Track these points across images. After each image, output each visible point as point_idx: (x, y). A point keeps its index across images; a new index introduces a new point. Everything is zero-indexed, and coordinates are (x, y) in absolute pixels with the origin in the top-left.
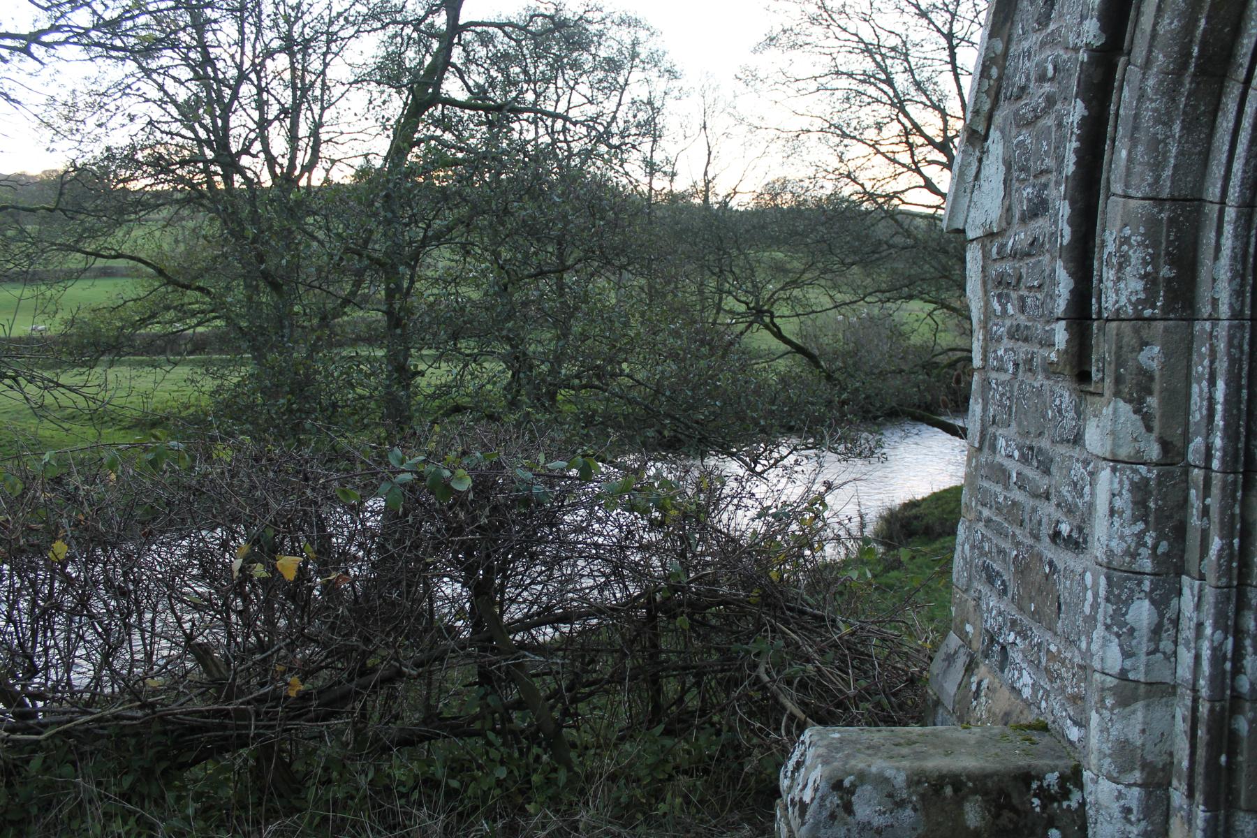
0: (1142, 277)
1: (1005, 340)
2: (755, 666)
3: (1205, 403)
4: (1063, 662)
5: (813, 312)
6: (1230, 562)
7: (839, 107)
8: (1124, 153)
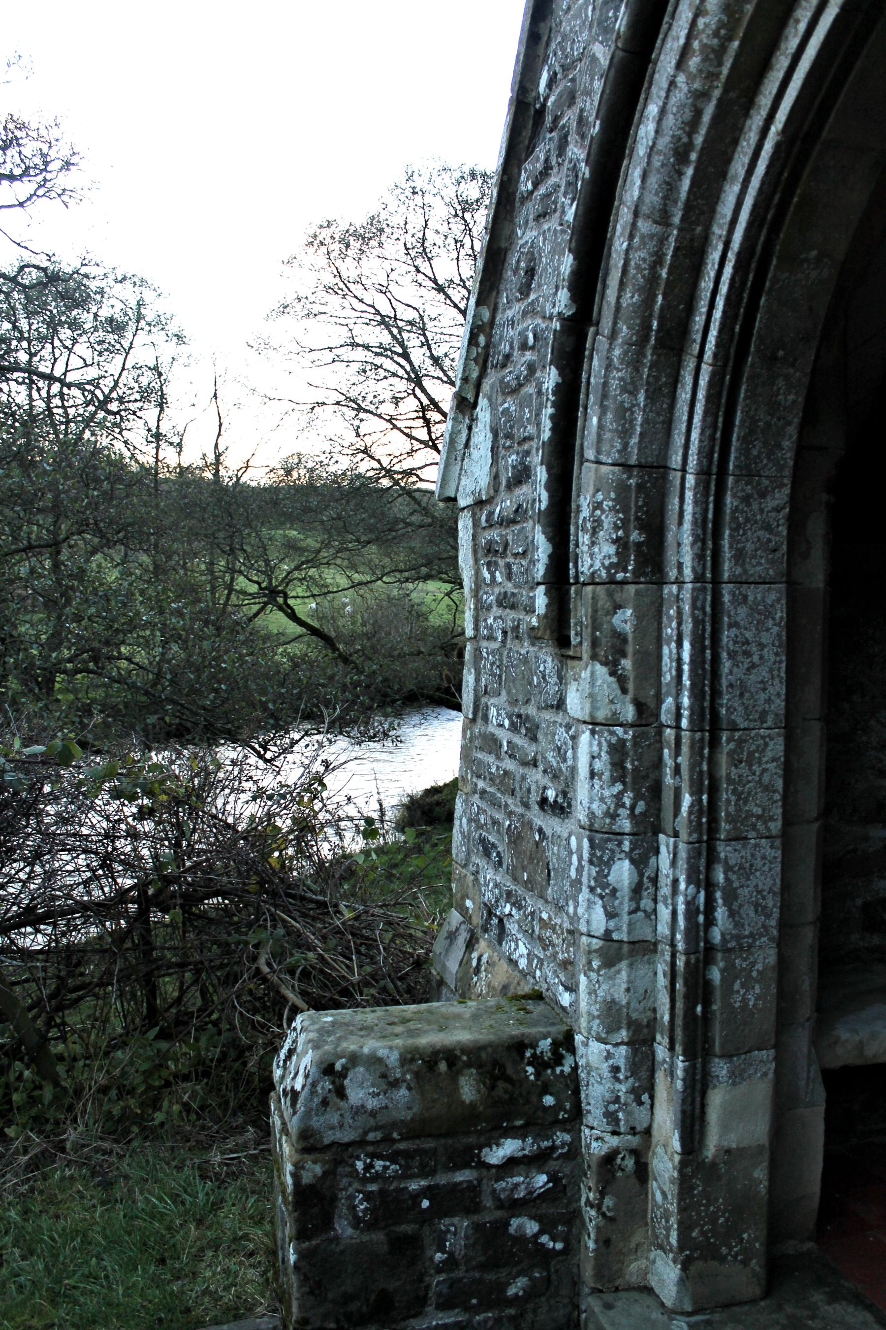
0: (614, 542)
1: (495, 608)
2: (254, 959)
3: (674, 664)
4: (553, 928)
5: (329, 592)
6: (699, 818)
7: (354, 379)
8: (595, 420)
